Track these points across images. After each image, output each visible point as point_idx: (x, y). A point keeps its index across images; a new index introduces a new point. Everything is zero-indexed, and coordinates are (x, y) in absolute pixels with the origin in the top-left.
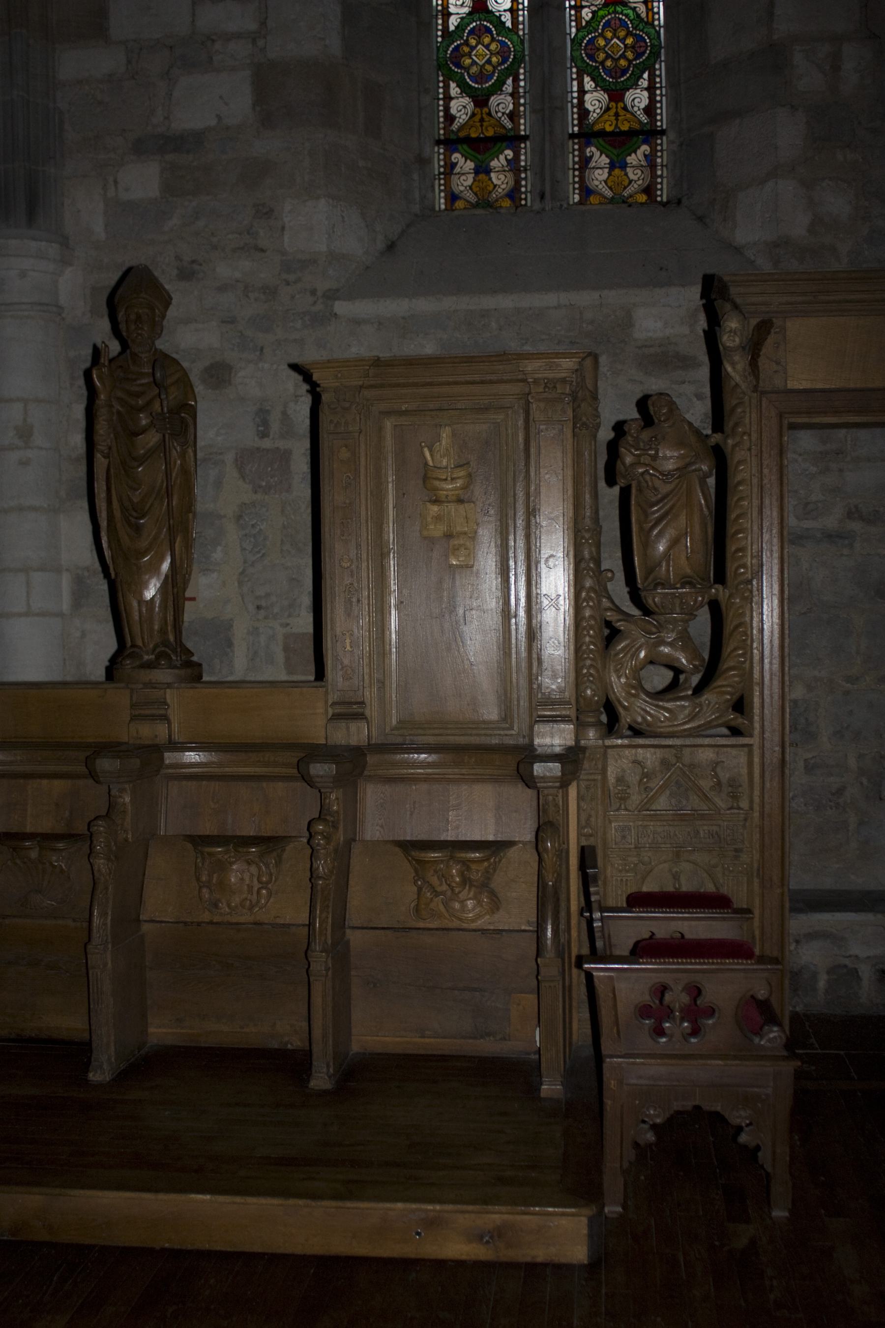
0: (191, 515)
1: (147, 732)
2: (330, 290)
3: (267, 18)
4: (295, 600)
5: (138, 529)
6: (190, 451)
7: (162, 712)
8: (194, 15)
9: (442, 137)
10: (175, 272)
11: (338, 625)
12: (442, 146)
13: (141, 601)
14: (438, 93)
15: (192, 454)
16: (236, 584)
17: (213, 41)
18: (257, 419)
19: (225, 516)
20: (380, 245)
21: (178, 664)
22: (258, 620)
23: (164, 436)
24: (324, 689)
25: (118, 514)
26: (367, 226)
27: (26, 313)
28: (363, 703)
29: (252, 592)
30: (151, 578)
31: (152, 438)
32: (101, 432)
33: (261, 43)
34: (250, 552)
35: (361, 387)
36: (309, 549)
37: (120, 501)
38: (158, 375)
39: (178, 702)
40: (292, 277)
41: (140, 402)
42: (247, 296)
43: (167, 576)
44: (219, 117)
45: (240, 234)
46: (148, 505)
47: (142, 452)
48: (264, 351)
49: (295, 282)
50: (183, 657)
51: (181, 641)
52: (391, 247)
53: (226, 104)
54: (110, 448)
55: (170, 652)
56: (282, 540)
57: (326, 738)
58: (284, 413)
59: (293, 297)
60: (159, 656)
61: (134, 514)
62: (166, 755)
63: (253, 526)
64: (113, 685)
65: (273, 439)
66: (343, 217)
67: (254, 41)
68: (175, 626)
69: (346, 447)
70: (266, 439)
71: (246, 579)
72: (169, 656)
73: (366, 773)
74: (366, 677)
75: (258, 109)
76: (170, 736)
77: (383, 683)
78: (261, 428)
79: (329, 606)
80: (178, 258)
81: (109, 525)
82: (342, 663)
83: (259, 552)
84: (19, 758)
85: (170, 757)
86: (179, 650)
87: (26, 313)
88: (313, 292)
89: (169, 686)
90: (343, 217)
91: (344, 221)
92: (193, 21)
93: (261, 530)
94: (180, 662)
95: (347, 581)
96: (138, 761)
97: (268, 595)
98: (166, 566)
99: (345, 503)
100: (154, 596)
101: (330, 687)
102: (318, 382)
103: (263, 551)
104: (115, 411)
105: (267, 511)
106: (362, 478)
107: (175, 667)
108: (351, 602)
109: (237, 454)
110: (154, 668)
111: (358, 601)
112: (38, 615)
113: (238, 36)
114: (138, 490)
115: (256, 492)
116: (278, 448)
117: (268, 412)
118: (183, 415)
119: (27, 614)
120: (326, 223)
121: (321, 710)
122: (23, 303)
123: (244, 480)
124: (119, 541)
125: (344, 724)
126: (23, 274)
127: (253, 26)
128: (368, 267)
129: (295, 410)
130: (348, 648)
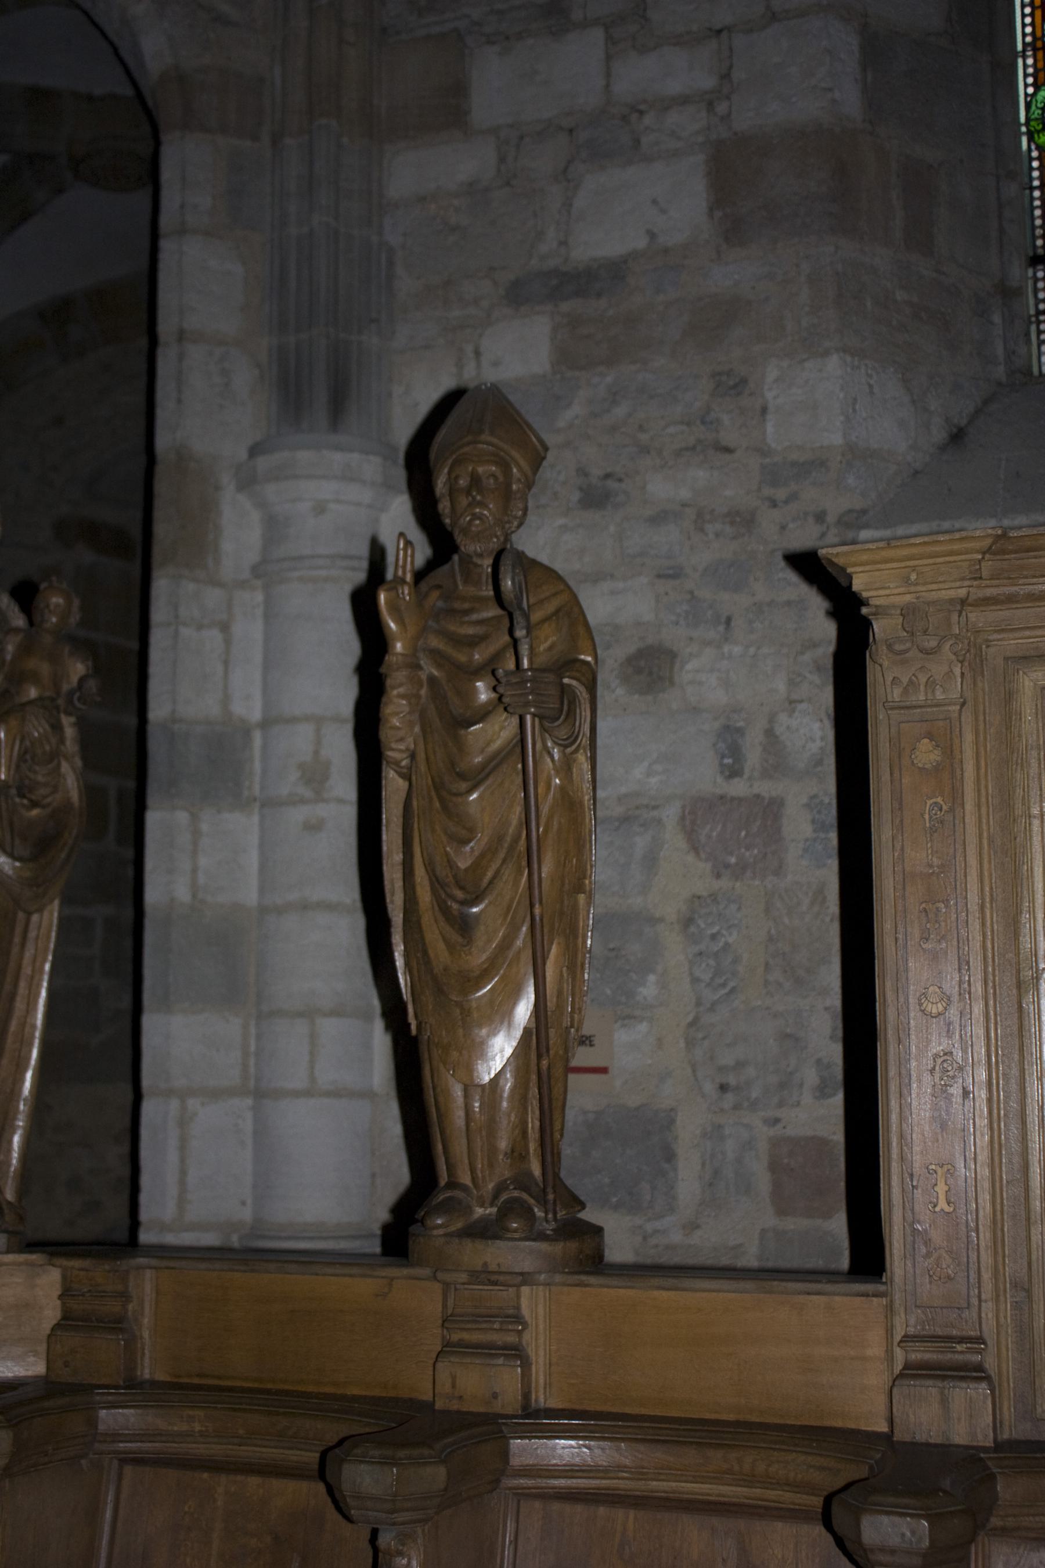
0: (582, 898)
1: (478, 1385)
2: (850, 511)
3: (731, 67)
4: (791, 1073)
5: (465, 926)
6: (582, 758)
7: (511, 1339)
8: (608, 75)
9: (1040, 252)
10: (576, 496)
11: (917, 1149)
12: (1041, 267)
13: (469, 1087)
14: (1031, 179)
15: (586, 767)
16: (682, 1044)
17: (641, 113)
18: (721, 745)
19: (661, 920)
20: (939, 434)
21: (549, 1228)
22: (722, 1110)
23: (522, 719)
24: (884, 1301)
25: (424, 895)
26: (914, 402)
27: (323, 573)
28: (980, 1340)
29: (712, 1058)
30: (494, 1033)
31: (499, 731)
32: (396, 722)
33: (722, 108)
34: (708, 985)
35: (963, 602)
36: (832, 975)
37: (430, 867)
38: (508, 584)
39: (549, 1314)
40: (781, 494)
41: (477, 657)
42: (702, 530)
43: (527, 1031)
44: (652, 235)
45: (688, 424)
46: (490, 874)
47: (478, 760)
48: (733, 624)
49: (786, 502)
50: (561, 1214)
51: (556, 1176)
52: (957, 437)
53: (663, 211)
54: (413, 756)
55: (532, 1201)
56: (767, 964)
57: (891, 1421)
58: (769, 733)
59: (783, 528)
60: (507, 1210)
61: (460, 894)
62: (516, 1443)
63: (713, 937)
64: (405, 1271)
65: (750, 778)
66: (871, 386)
67: (710, 106)
68: (542, 1144)
69: (930, 736)
70: (736, 780)
71: (700, 1035)
72: (530, 1210)
73: (995, 1521)
74: (986, 1276)
75: (718, 214)
76: (526, 1396)
77: (1029, 1292)
78: (728, 761)
79: (894, 1104)
80: (582, 472)
81: (406, 920)
82: (927, 1242)
83: (724, 985)
84: (197, 1427)
85: (525, 1450)
86: (551, 1197)
87: (323, 573)
88: (820, 517)
89: (526, 1278)
90: (871, 386)
91: (872, 393)
92: (608, 85)
93: (727, 944)
94: (553, 1225)
95: (936, 1048)
96: (442, 1471)
97: (740, 1065)
98: (523, 1010)
99: (931, 866)
100: (499, 1075)
101: (898, 1297)
102: (865, 594)
103: (732, 984)
104: (424, 677)
105: (739, 909)
106: (969, 806)
107: (541, 1237)
108: (949, 1098)
109: (684, 807)
110: (496, 1237)
111: (966, 1093)
112: (328, 1094)
113: (683, 100)
114: (470, 841)
115: (718, 876)
116: (758, 796)
117: (740, 731)
118: (566, 681)
119: (308, 1094)
120: (841, 395)
121: (876, 1349)
122: (319, 556)
123: (697, 853)
124: (425, 952)
125: (934, 1391)
126: (320, 509)
127: (709, 83)
128: (916, 472)
129: (788, 728)
130: (942, 1204)
